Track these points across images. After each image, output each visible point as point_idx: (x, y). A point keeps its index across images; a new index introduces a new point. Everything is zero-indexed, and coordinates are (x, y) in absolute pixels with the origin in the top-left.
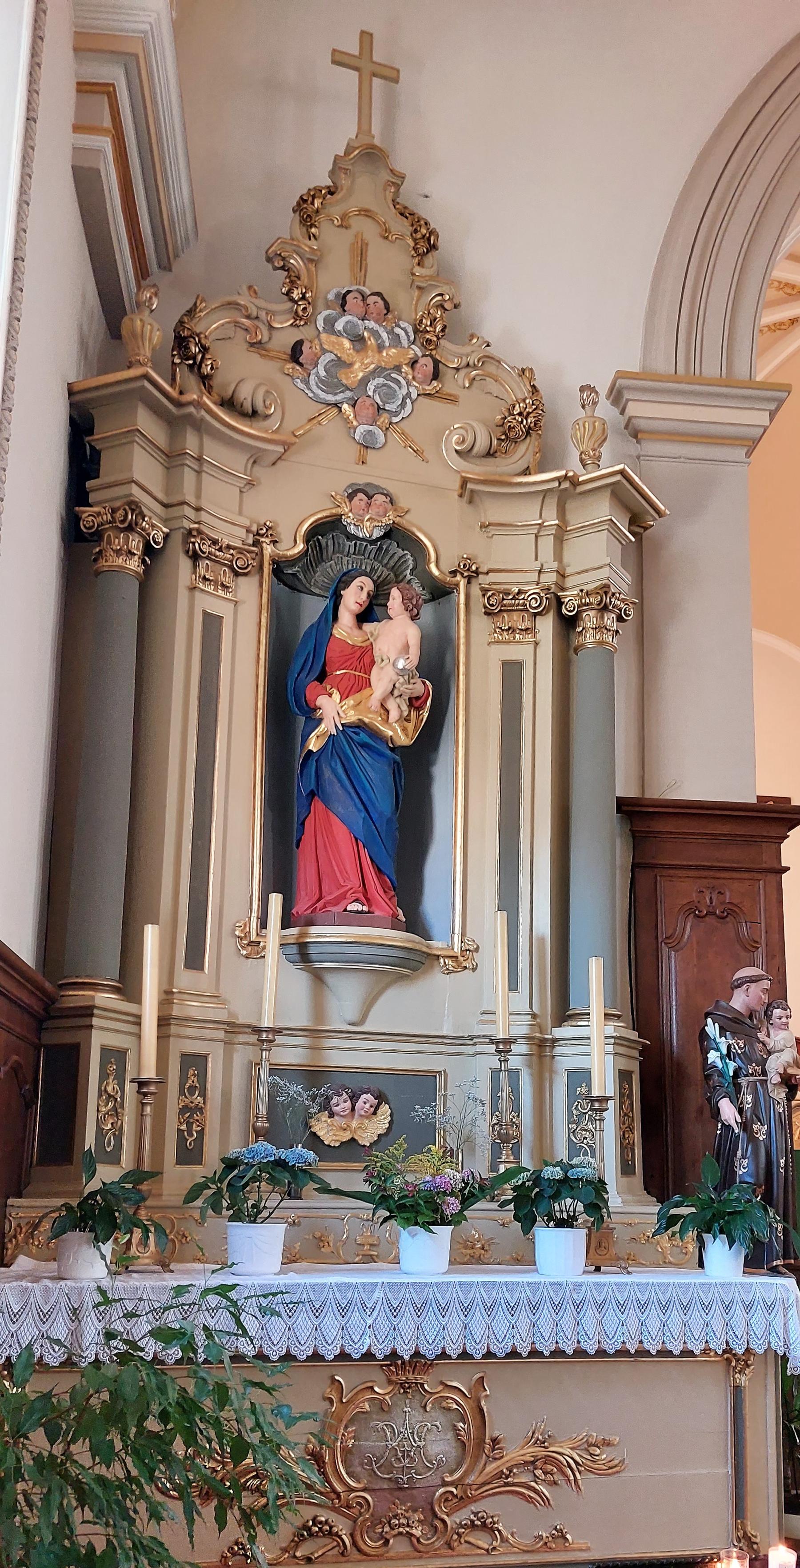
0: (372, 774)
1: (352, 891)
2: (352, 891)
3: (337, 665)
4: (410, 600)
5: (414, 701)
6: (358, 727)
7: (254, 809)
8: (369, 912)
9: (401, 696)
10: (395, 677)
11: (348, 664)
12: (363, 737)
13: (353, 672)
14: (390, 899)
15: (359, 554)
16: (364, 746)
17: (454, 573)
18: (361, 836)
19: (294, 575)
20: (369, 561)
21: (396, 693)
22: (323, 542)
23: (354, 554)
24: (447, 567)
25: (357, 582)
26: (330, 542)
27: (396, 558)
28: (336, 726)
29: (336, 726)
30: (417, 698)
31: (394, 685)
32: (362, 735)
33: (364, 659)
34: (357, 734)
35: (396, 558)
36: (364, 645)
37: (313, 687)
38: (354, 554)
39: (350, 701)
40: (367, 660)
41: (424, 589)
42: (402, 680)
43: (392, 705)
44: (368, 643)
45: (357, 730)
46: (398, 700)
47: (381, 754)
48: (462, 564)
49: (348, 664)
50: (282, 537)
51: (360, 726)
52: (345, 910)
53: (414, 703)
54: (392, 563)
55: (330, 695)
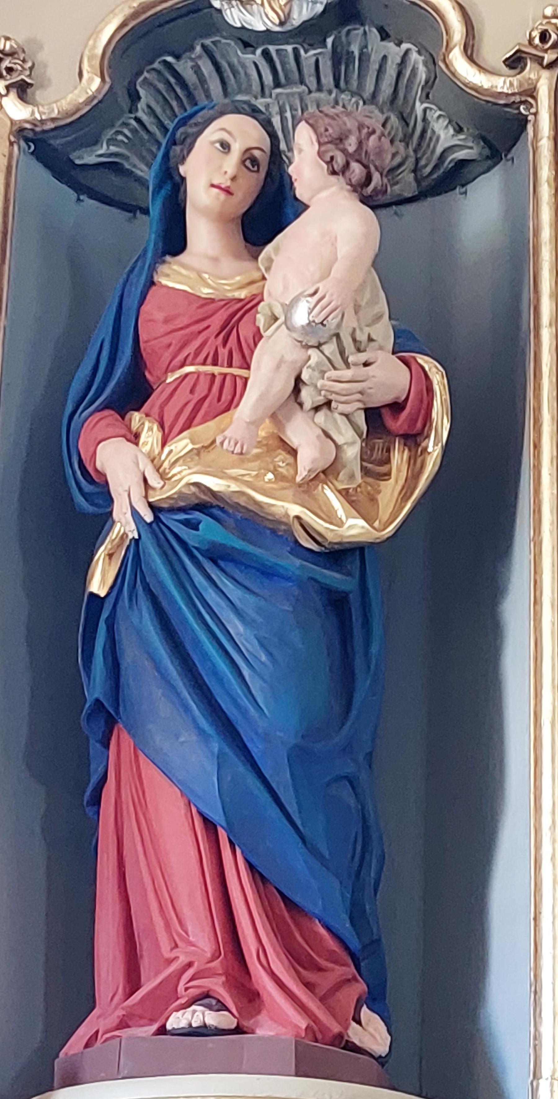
0: (236, 627)
1: (190, 972)
2: (190, 972)
3: (167, 355)
4: (339, 140)
5: (386, 415)
6: (202, 507)
7: (537, 993)
8: (238, 1030)
9: (328, 404)
10: (294, 354)
11: (191, 349)
12: (209, 531)
13: (209, 369)
14: (322, 1000)
15: (289, 82)
16: (217, 555)
17: (516, 62)
18: (217, 816)
19: (113, 166)
20: (322, 96)
21: (306, 395)
22: (184, 67)
23: (277, 84)
24: (496, 49)
25: (212, 134)
26: (207, 68)
27: (391, 71)
28: (135, 513)
29: (135, 513)
30: (396, 407)
31: (298, 380)
32: (206, 521)
33: (231, 328)
34: (194, 526)
35: (391, 71)
36: (242, 294)
37: (96, 423)
38: (277, 84)
39: (182, 444)
40: (245, 331)
41: (459, 130)
42: (315, 355)
43: (302, 433)
44: (253, 289)
45: (197, 515)
46: (321, 417)
47: (268, 573)
48: (536, 34)
49: (191, 349)
50: (51, 72)
51: (206, 505)
52: (162, 1031)
53: (386, 424)
54: (386, 89)
55: (135, 438)
